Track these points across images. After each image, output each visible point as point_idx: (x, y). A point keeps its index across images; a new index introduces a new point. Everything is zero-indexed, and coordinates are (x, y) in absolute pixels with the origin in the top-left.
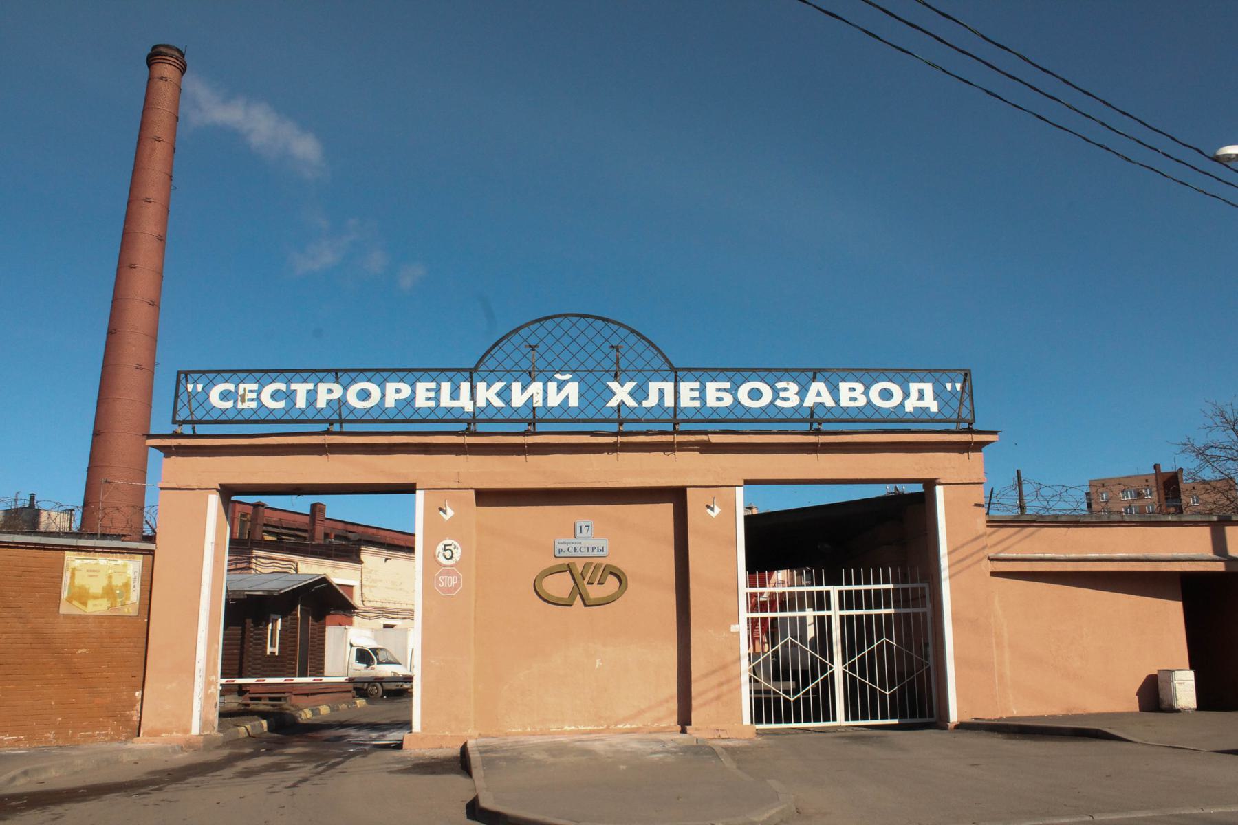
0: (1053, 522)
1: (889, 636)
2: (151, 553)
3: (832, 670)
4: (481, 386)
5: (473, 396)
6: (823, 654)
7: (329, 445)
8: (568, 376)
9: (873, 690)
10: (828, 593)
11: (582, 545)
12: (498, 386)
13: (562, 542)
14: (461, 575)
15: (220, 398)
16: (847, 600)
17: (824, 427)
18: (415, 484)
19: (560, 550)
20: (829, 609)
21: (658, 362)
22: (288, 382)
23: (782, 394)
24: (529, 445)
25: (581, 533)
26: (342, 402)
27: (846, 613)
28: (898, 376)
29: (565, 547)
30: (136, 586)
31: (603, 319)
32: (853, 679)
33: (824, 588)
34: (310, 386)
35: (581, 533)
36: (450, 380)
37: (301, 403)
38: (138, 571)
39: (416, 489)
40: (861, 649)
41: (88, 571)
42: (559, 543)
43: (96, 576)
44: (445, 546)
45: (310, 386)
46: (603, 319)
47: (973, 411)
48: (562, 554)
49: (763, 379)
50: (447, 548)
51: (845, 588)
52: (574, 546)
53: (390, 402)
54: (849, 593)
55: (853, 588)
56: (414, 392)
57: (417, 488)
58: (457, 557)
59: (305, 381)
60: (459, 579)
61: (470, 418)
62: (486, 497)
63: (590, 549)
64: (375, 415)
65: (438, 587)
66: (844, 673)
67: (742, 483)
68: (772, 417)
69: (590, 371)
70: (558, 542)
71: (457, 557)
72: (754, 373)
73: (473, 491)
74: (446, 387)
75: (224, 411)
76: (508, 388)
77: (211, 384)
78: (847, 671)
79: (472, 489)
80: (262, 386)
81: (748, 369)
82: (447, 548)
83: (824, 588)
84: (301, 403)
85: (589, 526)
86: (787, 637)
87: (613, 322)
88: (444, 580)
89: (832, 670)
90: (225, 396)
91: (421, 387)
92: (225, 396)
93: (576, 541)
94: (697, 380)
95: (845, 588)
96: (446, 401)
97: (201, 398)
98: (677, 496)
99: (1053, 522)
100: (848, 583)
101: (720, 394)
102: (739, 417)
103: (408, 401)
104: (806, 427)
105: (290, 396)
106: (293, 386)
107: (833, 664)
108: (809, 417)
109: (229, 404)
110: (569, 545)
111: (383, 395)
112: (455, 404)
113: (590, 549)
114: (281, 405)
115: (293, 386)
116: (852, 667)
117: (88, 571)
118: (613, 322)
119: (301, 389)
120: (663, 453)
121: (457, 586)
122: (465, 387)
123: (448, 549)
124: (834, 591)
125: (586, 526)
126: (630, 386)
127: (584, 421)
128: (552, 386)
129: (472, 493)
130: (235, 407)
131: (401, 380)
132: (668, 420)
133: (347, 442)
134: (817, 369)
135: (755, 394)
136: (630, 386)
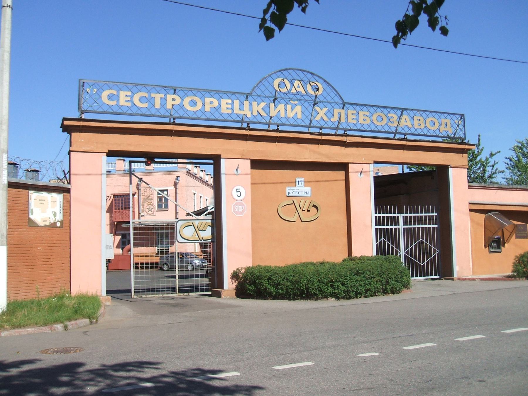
0: (480, 187)
1: (384, 237)
2: (68, 191)
3: (400, 254)
4: (255, 104)
5: (251, 110)
6: (396, 247)
7: (175, 130)
8: (296, 102)
9: (416, 263)
10: (398, 217)
11: (300, 191)
12: (263, 105)
13: (290, 189)
14: (246, 205)
15: (108, 98)
16: (407, 221)
17: (177, 121)
18: (221, 155)
19: (289, 193)
20: (399, 225)
21: (337, 99)
22: (149, 92)
23: (129, 99)
24: (280, 137)
25: (298, 184)
26: (181, 106)
27: (406, 227)
28: (365, 108)
29: (291, 192)
30: (61, 210)
31: (312, 74)
32: (408, 258)
33: (396, 215)
34: (162, 96)
35: (298, 184)
36: (238, 99)
37: (157, 105)
38: (61, 201)
39: (402, 165)
40: (411, 245)
41: (40, 200)
42: (288, 189)
43: (43, 204)
44: (237, 189)
45: (162, 96)
46: (312, 74)
47: (465, 134)
48: (290, 195)
49: (434, 117)
50: (238, 190)
51: (405, 215)
52: (295, 191)
53: (207, 108)
54: (407, 217)
55: (408, 215)
56: (220, 105)
57: (222, 157)
58: (243, 196)
59: (158, 92)
60: (245, 207)
61: (241, 120)
62: (256, 164)
63: (303, 193)
64: (199, 115)
65: (234, 211)
66: (405, 255)
67: (373, 162)
68: (373, 130)
69: (258, 96)
70: (288, 189)
71: (243, 196)
72: (379, 109)
73: (250, 160)
74: (237, 103)
75: (110, 107)
76: (268, 106)
77: (101, 89)
78: (406, 254)
79: (249, 159)
80: (133, 94)
81: (376, 106)
82: (238, 190)
83: (396, 215)
84: (157, 105)
85: (302, 181)
86: (382, 238)
87: (316, 75)
88: (237, 208)
89: (400, 254)
90: (110, 97)
91: (224, 101)
92: (110, 97)
93: (297, 189)
94: (229, 98)
95: (405, 215)
96: (237, 111)
97: (96, 97)
98: (344, 167)
99: (480, 187)
100: (407, 213)
101: (365, 117)
102: (95, 110)
103: (183, 108)
104: (392, 136)
105: (150, 100)
106: (153, 95)
107: (400, 251)
108: (309, 125)
109: (114, 103)
110: (293, 191)
111: (204, 105)
112: (242, 112)
113: (303, 193)
114: (144, 105)
115: (153, 95)
116: (408, 252)
117: (40, 200)
118: (316, 75)
119: (158, 97)
120: (245, 141)
121: (244, 210)
122: (247, 103)
123: (238, 191)
124: (401, 216)
125: (301, 181)
126: (325, 110)
127: (130, 114)
128: (289, 107)
129: (249, 162)
130: (118, 105)
131: (212, 97)
132: (334, 128)
133: (114, 126)
134: (404, 108)
135: (193, 103)
136: (325, 110)
